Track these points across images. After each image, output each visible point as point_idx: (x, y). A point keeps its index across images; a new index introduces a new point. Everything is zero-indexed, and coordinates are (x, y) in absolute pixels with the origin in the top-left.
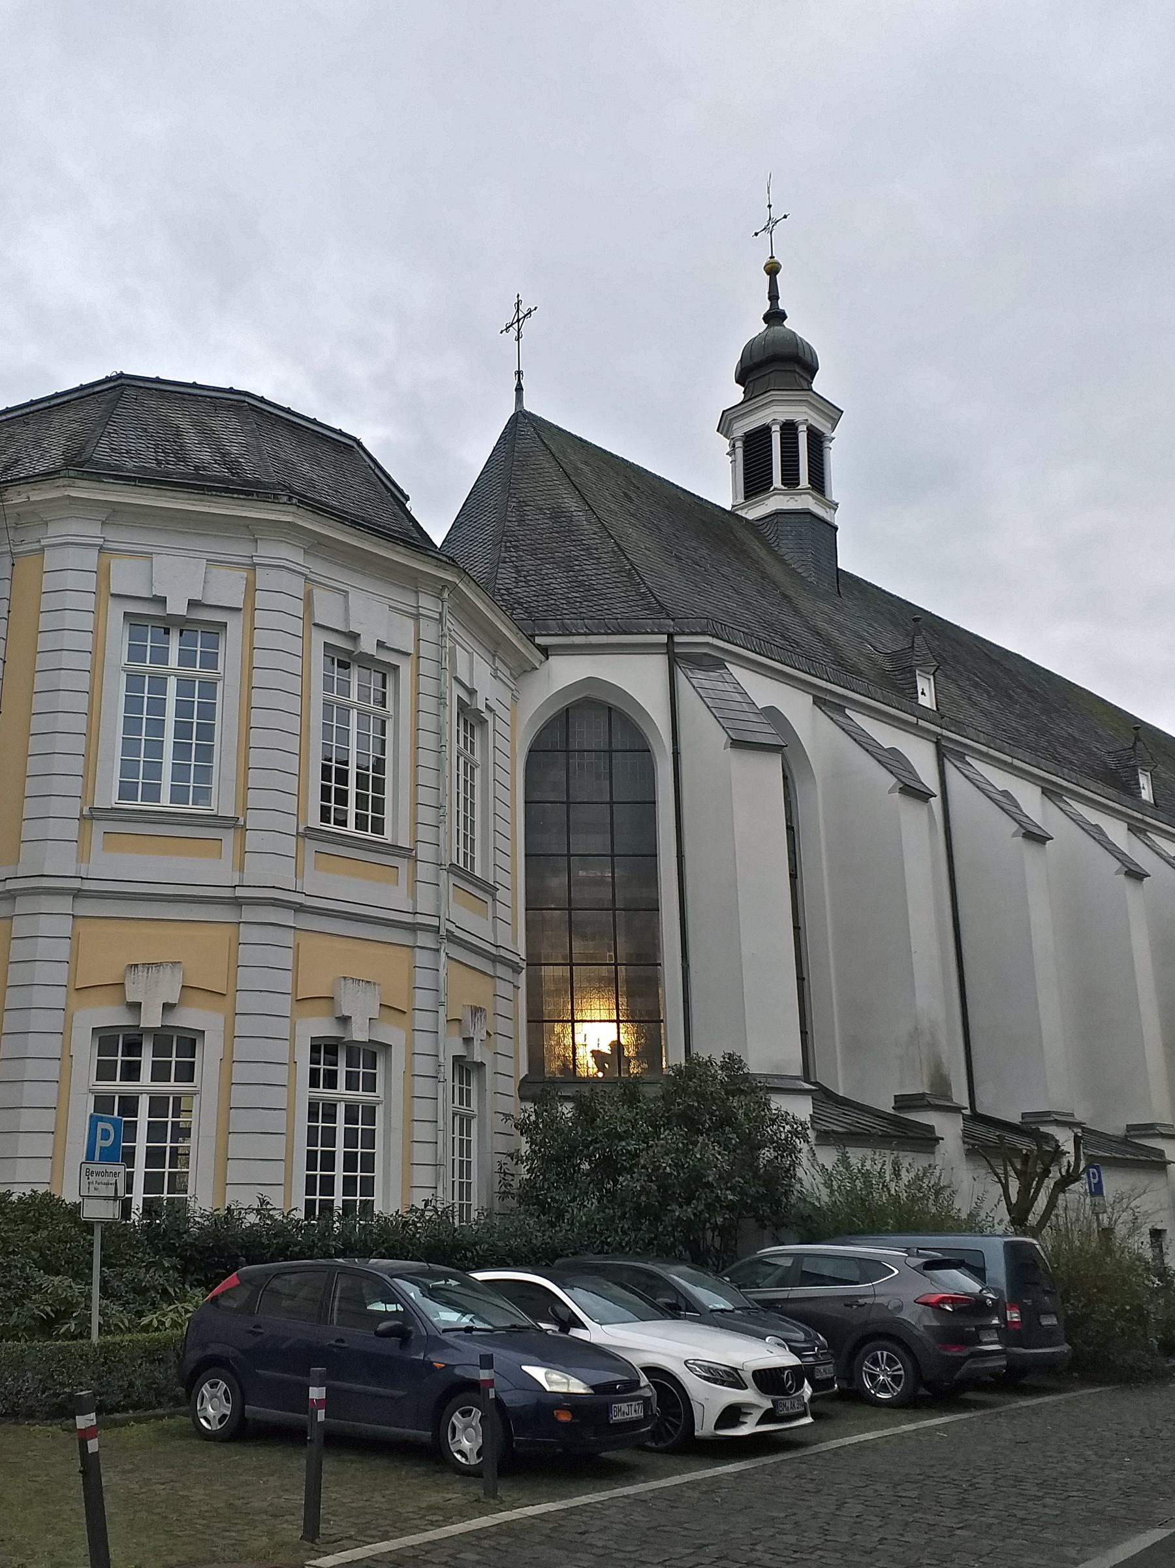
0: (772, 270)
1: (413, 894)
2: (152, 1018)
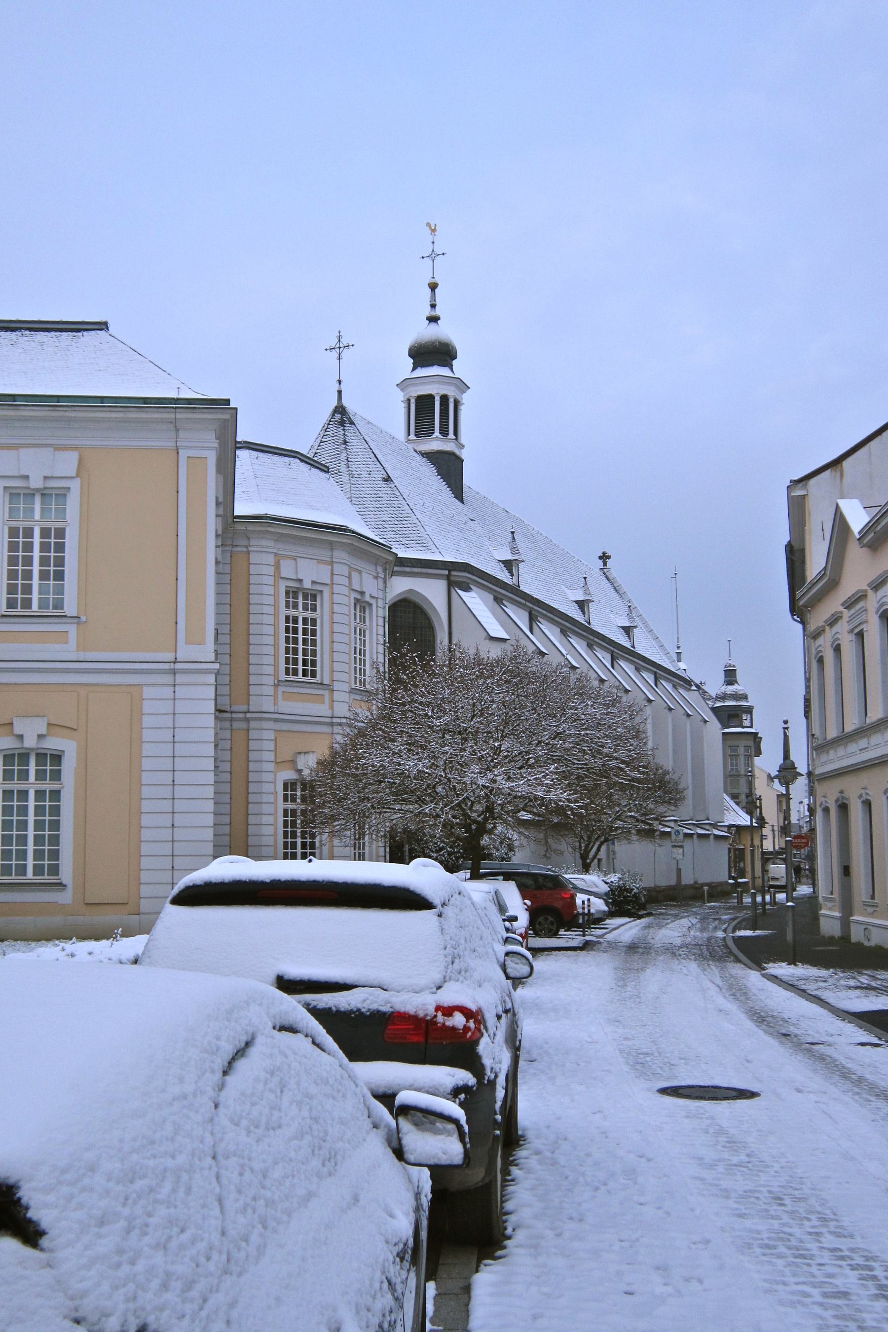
0: (433, 287)
1: (332, 708)
2: (30, 742)
